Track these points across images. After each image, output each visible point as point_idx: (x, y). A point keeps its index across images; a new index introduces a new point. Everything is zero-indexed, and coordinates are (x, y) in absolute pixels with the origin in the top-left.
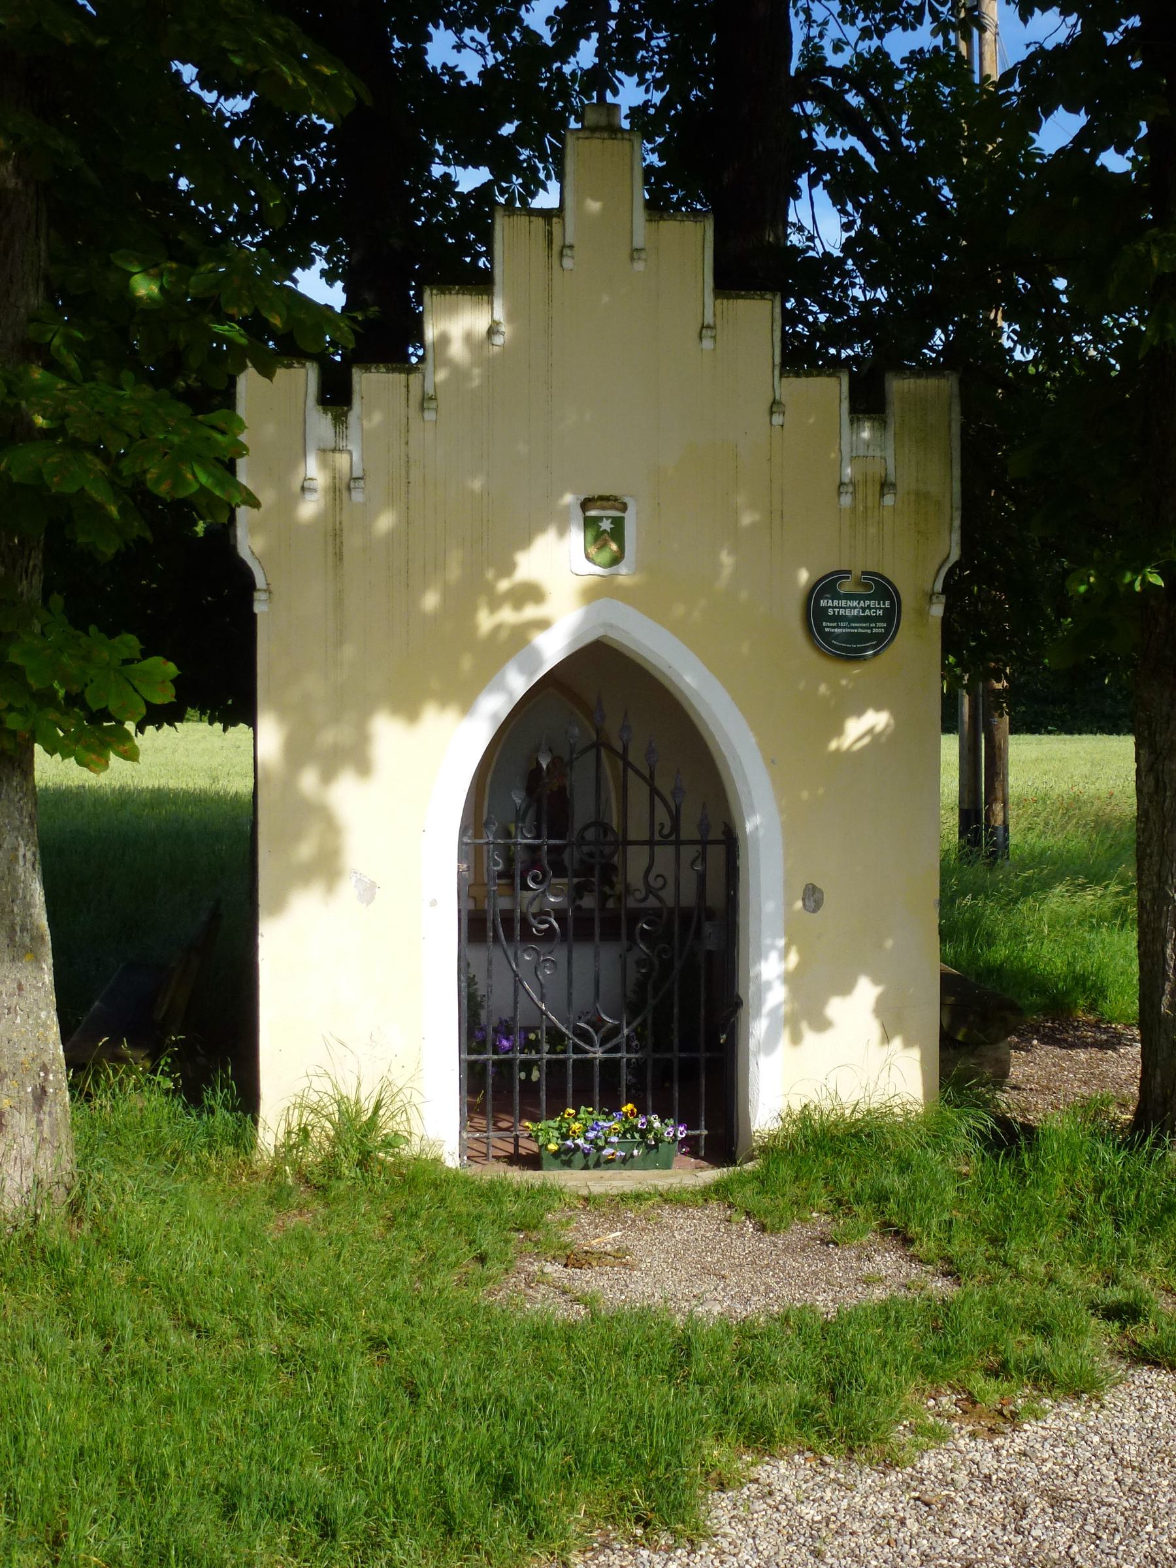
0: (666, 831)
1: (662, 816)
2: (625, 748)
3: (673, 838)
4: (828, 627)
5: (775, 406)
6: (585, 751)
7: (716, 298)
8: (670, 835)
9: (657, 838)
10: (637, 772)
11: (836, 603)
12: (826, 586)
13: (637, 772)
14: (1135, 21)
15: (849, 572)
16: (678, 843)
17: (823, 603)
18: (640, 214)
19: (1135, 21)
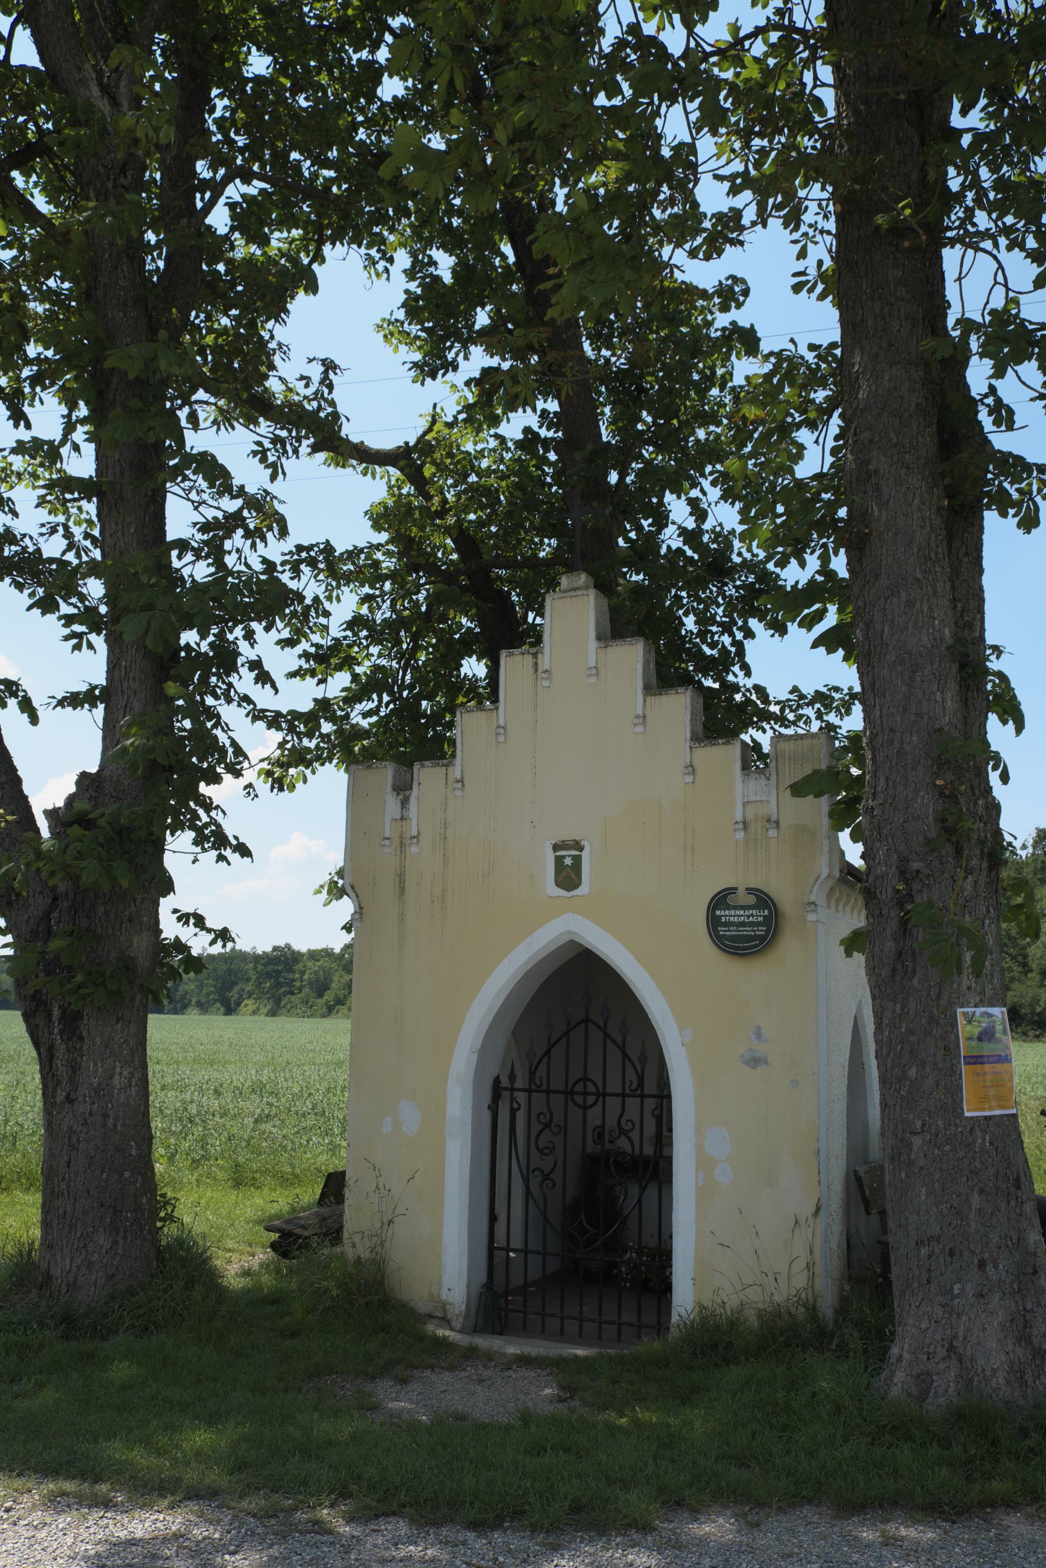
0: (634, 1087)
1: (631, 1075)
2: (606, 1024)
3: (639, 1092)
4: (722, 931)
5: (691, 768)
6: (579, 1024)
7: (645, 695)
8: (636, 1090)
9: (627, 1091)
10: (613, 1041)
11: (727, 912)
12: (721, 900)
13: (613, 1041)
14: (192, 804)
15: (736, 889)
16: (643, 1096)
17: (718, 913)
18: (592, 644)
19: (192, 804)
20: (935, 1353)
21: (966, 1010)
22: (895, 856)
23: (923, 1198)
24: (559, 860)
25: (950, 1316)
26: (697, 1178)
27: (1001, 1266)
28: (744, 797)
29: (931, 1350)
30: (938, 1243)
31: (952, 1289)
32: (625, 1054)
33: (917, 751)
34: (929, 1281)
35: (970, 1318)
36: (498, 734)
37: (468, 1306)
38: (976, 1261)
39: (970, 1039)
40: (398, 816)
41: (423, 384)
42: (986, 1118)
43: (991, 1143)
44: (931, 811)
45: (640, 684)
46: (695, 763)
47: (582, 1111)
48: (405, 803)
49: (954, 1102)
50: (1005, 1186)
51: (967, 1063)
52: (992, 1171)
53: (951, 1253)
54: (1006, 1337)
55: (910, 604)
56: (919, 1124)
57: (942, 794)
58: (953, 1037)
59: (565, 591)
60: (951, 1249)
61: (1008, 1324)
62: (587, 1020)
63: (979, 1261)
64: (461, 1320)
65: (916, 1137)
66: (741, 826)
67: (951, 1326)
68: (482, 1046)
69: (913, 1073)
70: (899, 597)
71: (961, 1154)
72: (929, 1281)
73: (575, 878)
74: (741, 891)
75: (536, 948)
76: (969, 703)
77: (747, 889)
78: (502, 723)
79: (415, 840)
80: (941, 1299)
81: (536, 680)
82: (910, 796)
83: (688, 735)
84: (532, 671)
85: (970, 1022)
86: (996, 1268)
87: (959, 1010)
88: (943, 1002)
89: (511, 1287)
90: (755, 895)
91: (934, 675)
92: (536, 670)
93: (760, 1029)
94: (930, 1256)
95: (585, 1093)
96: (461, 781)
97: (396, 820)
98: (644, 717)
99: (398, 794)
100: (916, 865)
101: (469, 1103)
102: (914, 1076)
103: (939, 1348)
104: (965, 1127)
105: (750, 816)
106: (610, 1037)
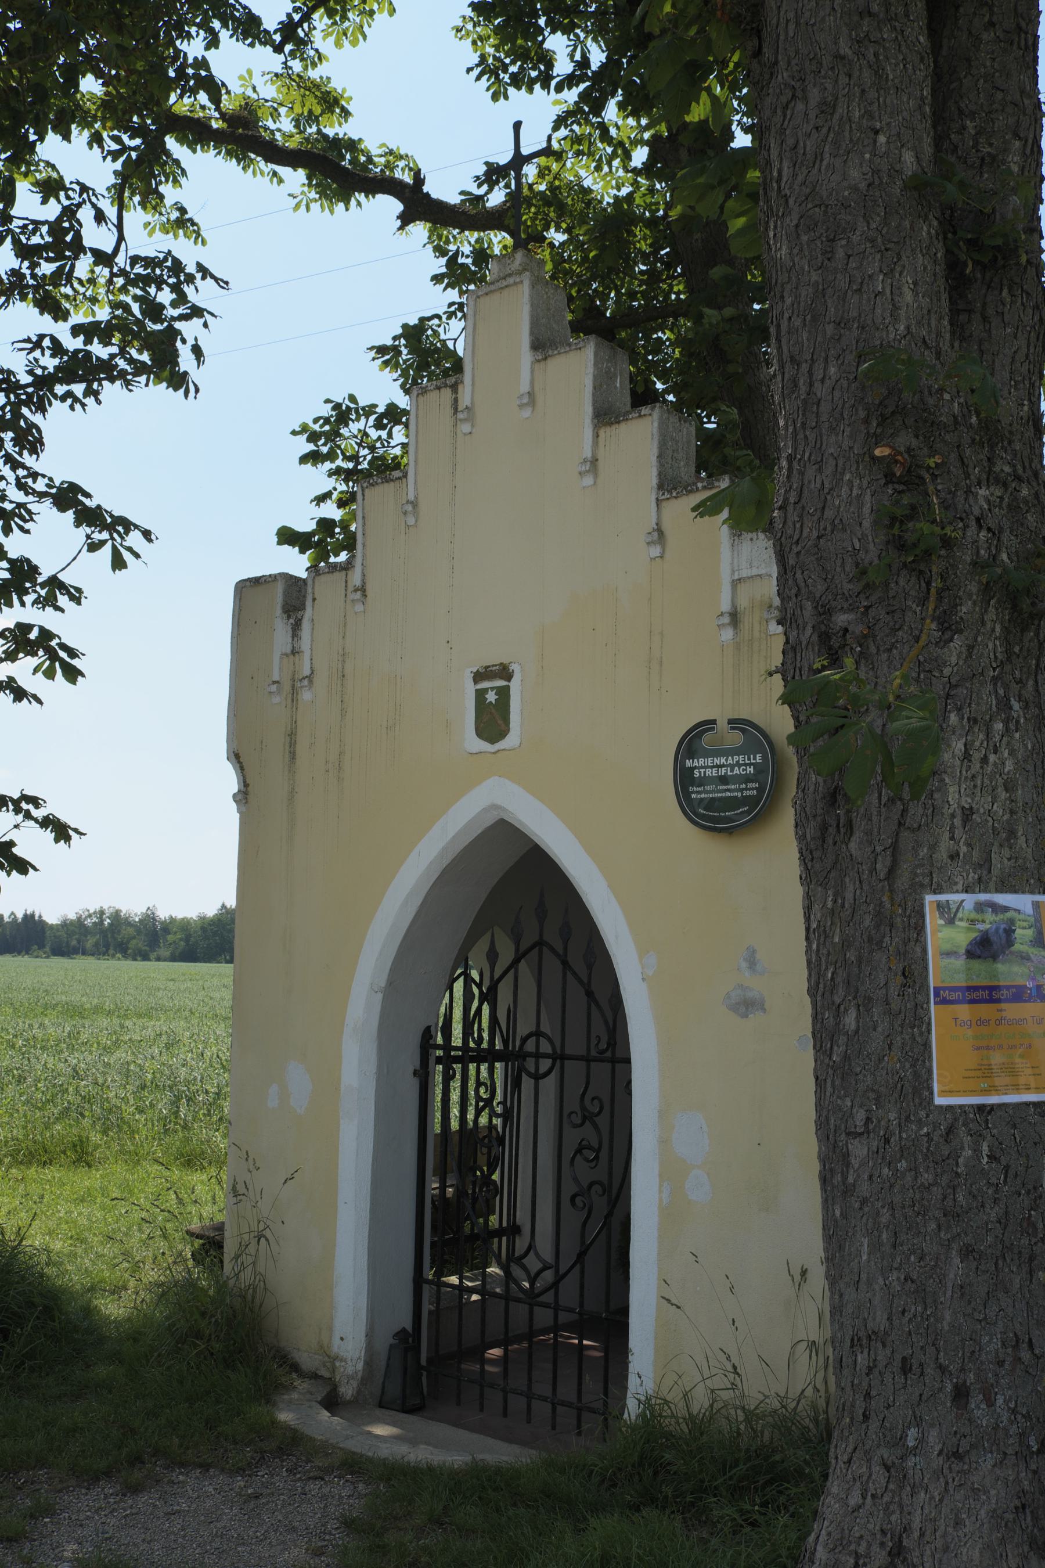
0: (603, 1045)
3: (608, 1054)
5: (659, 534)
10: (575, 974)
11: (702, 761)
13: (575, 974)
15: (714, 722)
17: (689, 763)
18: (526, 356)
20: (868, 1555)
21: (942, 898)
22: (809, 605)
23: (865, 1257)
24: (480, 694)
25: (902, 1488)
26: (660, 1192)
27: (1000, 1400)
28: (733, 572)
29: (862, 1550)
30: (884, 1345)
31: (903, 1437)
32: (589, 994)
33: (837, 394)
34: (866, 1417)
35: (932, 1498)
36: (405, 513)
37: (369, 1364)
38: (949, 1387)
39: (949, 954)
40: (289, 650)
41: (506, 98)
42: (981, 1108)
43: (992, 1157)
44: (866, 510)
45: (589, 409)
46: (666, 526)
47: (533, 1081)
48: (296, 629)
49: (916, 1075)
50: (1025, 1241)
51: (942, 1001)
52: (994, 1213)
53: (906, 1368)
54: (1003, 1541)
55: (827, 108)
56: (860, 1116)
57: (889, 478)
58: (918, 950)
59: (492, 283)
60: (904, 1359)
61: (1010, 1516)
62: (540, 944)
63: (956, 1387)
64: (355, 1384)
65: (856, 1142)
66: (726, 620)
67: (901, 1506)
68: (390, 983)
69: (850, 1020)
70: (805, 99)
71: (927, 1177)
72: (866, 1417)
73: (500, 722)
74: (722, 724)
75: (451, 834)
76: (990, 311)
77: (730, 722)
78: (411, 497)
79: (306, 682)
80: (885, 1452)
81: (455, 425)
82: (827, 486)
83: (655, 481)
84: (449, 411)
85: (951, 922)
86: (991, 1403)
87: (929, 899)
88: (902, 882)
89: (510, 1334)
90: (743, 731)
91: (873, 241)
92: (456, 410)
93: (754, 951)
94: (870, 1370)
95: (538, 1056)
96: (362, 590)
97: (286, 655)
98: (594, 461)
99: (289, 617)
100: (842, 619)
101: (372, 1068)
102: (853, 1027)
103: (875, 1548)
104: (936, 1126)
105: (743, 603)
106: (571, 969)
